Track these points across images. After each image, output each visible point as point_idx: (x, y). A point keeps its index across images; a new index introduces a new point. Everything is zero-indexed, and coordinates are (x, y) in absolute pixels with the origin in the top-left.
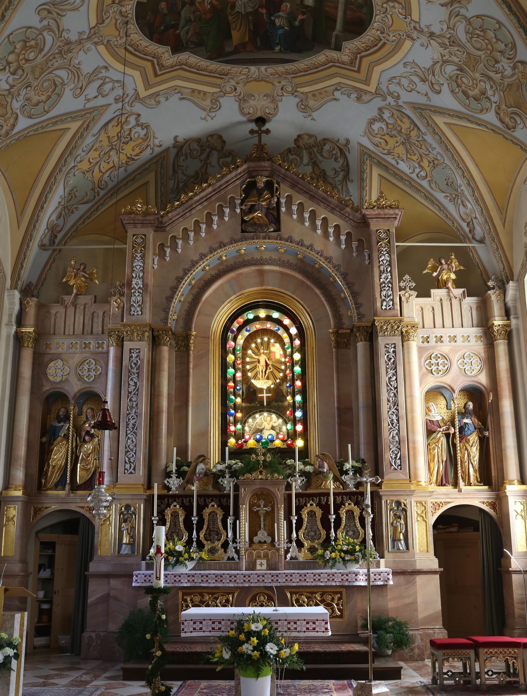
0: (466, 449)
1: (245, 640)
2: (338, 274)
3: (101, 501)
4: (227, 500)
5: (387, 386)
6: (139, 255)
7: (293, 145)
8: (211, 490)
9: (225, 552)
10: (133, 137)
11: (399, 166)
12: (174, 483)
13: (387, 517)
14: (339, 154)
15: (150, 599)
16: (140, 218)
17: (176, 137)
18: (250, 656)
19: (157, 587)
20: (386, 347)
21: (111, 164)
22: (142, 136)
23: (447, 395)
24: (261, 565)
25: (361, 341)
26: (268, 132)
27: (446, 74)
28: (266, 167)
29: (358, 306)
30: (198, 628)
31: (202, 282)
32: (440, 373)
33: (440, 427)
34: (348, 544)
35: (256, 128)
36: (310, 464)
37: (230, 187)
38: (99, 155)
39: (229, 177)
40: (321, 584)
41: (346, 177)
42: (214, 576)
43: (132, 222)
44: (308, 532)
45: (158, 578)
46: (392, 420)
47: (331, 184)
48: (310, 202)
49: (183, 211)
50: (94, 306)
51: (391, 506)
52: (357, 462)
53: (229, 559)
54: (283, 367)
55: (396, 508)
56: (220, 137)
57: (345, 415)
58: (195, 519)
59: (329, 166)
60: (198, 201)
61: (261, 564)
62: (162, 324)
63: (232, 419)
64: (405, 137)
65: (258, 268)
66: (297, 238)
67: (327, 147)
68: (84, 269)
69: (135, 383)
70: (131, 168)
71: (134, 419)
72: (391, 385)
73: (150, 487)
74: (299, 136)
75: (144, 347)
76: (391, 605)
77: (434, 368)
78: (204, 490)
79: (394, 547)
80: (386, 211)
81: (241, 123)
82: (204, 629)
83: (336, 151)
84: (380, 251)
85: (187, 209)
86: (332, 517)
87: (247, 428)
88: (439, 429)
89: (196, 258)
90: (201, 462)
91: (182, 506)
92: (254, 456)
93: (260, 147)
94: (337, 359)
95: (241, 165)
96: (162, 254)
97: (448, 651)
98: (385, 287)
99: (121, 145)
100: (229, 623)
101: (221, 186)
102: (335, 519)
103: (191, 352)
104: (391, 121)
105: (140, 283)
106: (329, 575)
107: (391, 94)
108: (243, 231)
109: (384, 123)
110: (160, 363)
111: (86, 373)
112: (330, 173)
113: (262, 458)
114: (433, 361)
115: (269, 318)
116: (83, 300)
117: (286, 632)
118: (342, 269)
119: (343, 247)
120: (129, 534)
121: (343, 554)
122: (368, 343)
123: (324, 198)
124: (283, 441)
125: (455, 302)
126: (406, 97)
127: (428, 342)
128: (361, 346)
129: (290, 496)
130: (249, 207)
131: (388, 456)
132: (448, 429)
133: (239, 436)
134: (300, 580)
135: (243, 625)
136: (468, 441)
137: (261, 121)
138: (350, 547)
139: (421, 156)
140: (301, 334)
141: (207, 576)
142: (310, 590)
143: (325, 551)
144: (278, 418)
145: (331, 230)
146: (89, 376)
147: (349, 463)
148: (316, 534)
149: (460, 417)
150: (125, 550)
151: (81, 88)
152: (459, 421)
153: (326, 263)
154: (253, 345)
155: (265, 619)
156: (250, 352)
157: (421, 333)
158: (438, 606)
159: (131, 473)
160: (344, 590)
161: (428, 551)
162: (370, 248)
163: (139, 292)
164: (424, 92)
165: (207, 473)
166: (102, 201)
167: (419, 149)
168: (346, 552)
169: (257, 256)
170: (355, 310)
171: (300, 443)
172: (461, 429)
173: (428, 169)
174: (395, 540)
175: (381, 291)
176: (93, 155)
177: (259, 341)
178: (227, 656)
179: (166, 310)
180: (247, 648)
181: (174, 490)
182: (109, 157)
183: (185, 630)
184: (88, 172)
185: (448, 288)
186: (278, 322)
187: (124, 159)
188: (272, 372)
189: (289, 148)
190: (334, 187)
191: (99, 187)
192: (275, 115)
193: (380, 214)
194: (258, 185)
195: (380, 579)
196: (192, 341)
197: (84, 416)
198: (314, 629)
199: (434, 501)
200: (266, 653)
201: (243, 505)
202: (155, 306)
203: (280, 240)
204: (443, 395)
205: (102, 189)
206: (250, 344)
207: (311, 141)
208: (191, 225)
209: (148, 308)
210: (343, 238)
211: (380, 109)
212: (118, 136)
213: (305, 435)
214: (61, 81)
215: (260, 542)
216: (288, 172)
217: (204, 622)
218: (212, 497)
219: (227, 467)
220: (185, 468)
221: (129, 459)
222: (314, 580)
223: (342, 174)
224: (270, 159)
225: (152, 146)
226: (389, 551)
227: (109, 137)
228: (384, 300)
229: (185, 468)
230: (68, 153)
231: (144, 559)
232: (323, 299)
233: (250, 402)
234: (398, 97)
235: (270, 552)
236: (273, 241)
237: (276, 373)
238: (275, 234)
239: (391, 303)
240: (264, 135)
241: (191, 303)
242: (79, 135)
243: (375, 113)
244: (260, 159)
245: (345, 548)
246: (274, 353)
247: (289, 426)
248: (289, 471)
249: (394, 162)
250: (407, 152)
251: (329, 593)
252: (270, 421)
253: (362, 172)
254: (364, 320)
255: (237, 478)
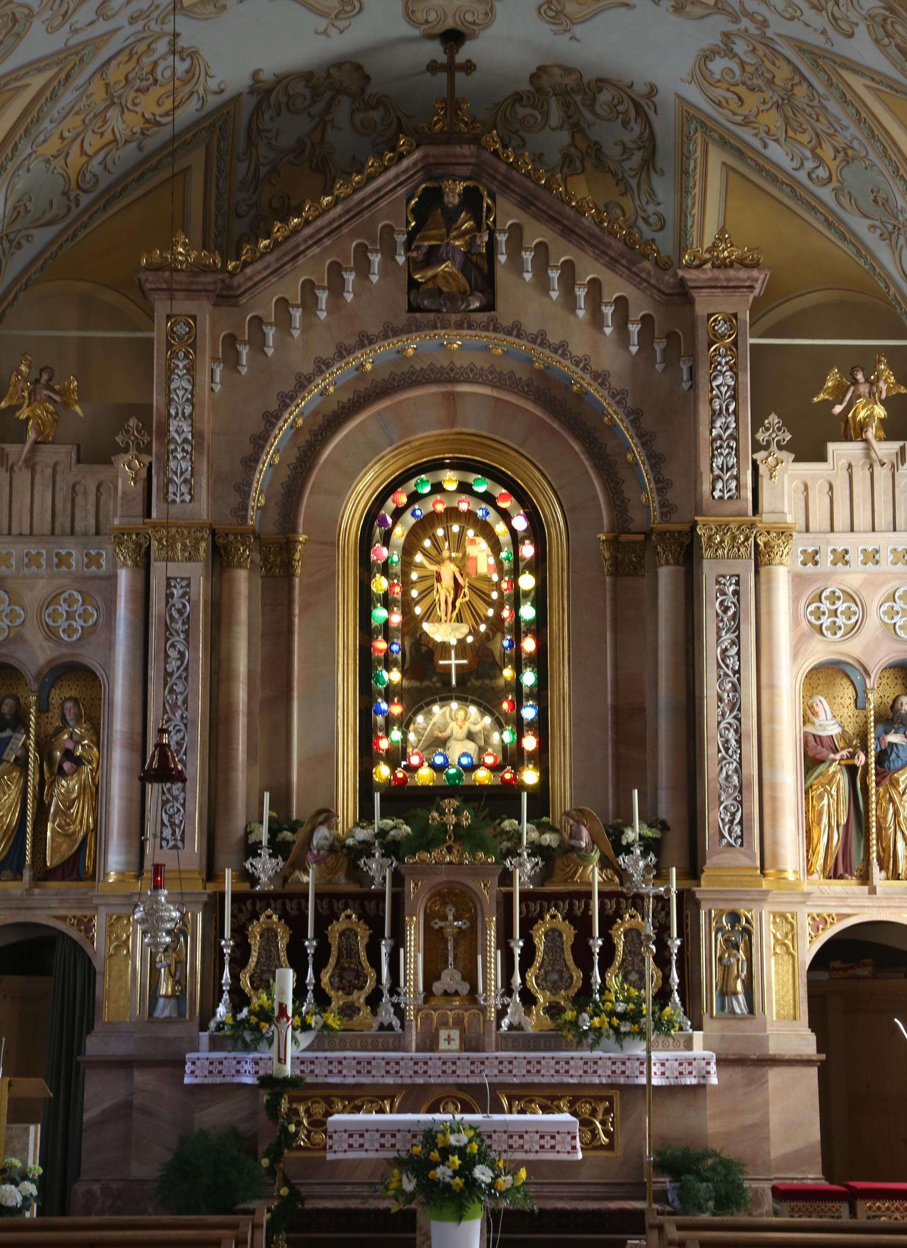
0: (891, 800)
1: (439, 1160)
2: (620, 411)
3: (161, 919)
4: (377, 905)
5: (719, 666)
6: (181, 365)
7: (526, 87)
8: (343, 884)
9: (374, 1012)
10: (159, 77)
11: (768, 153)
12: (265, 867)
13: (710, 945)
14: (632, 114)
15: (266, 1098)
16: (182, 277)
17: (255, 74)
18: (448, 1186)
19: (281, 1076)
20: (718, 582)
21: (108, 137)
22: (180, 72)
23: (857, 678)
24: (449, 1041)
25: (667, 563)
26: (469, 67)
27: (861, 8)
28: (464, 156)
29: (662, 485)
30: (356, 1145)
31: (319, 419)
32: (840, 633)
33: (836, 751)
34: (627, 1000)
35: (443, 58)
36: (552, 829)
37: (383, 204)
38: (84, 121)
39: (381, 180)
40: (571, 1081)
41: (649, 163)
42: (354, 1063)
43: (164, 286)
44: (546, 973)
45: (282, 1060)
46: (727, 741)
47: (614, 175)
48: (562, 242)
49: (277, 260)
50: (76, 468)
51: (719, 921)
52: (650, 826)
53: (382, 1027)
54: (495, 595)
55: (728, 927)
56: (359, 68)
57: (627, 726)
58: (310, 945)
59: (612, 136)
60: (311, 236)
61: (449, 1040)
62: (234, 521)
63: (380, 719)
64: (782, 93)
65: (443, 389)
66: (531, 328)
67: (605, 96)
68: (50, 380)
69: (180, 653)
70: (152, 143)
71: (179, 731)
72: (727, 666)
73: (212, 874)
74: (542, 69)
75: (195, 573)
76: (714, 1126)
77: (826, 621)
78: (329, 882)
79: (722, 1007)
80: (731, 273)
81: (405, 40)
82: (366, 1146)
83: (626, 106)
84: (713, 363)
85: (285, 254)
86: (597, 944)
87: (412, 737)
88: (832, 756)
89: (307, 368)
90: (321, 823)
91: (284, 915)
92: (435, 814)
93: (452, 104)
94: (615, 600)
95: (410, 153)
96: (231, 361)
97: (800, 1204)
98: (721, 447)
99: (132, 94)
100: (409, 1136)
101: (363, 200)
102: (601, 948)
103: (297, 580)
104: (749, 59)
105: (187, 428)
106: (586, 1063)
107: (751, 16)
108: (412, 309)
109: (736, 59)
110: (232, 607)
111: (62, 623)
112: (612, 151)
113: (453, 819)
114: (826, 606)
115: (464, 488)
116: (49, 454)
117: (505, 1151)
118: (629, 402)
119: (634, 349)
120: (173, 976)
121: (615, 1021)
122: (682, 569)
123: (593, 235)
124: (495, 769)
125: (882, 474)
126: (777, 26)
127: (816, 563)
128: (666, 576)
129: (509, 897)
130: (424, 250)
131: (715, 816)
132: (852, 755)
133: (396, 757)
134: (529, 1071)
135: (434, 1138)
136: (895, 784)
137: (453, 38)
138: (631, 1006)
139: (817, 135)
140: (537, 532)
141: (340, 1063)
142: (547, 1093)
143: (579, 1013)
144: (483, 715)
145: (608, 311)
146: (69, 630)
147: (633, 827)
148: (561, 977)
149: (881, 728)
150: (164, 1010)
151: (64, 16)
152: (877, 738)
153: (595, 385)
154: (427, 543)
155: (471, 1127)
156: (419, 558)
157: (800, 543)
158: (814, 1133)
159: (175, 847)
160: (617, 1095)
161: (795, 1018)
162: (693, 354)
163: (183, 450)
164: (821, 28)
165: (336, 847)
166: (85, 218)
167: (813, 122)
168: (622, 1016)
169: (443, 361)
170: (655, 495)
171: (530, 776)
172: (883, 757)
173: (833, 165)
174: (726, 993)
175: (713, 456)
176: (74, 122)
177: (440, 532)
178: (409, 1185)
179: (244, 488)
180: (442, 1173)
181: (265, 883)
182: (105, 122)
183: (335, 1147)
184: (55, 157)
185: (866, 441)
186: (488, 498)
187: (137, 123)
188: (469, 604)
189: (516, 93)
190: (620, 180)
191: (79, 187)
192: (488, 25)
193: (716, 279)
194: (446, 199)
195: (690, 1073)
196: (297, 556)
197: (55, 712)
198: (553, 1147)
199: (815, 911)
200: (475, 1180)
201: (411, 916)
202: (216, 478)
203: (495, 330)
204: (848, 677)
205: (86, 191)
206: (421, 540)
207: (570, 81)
208: (295, 294)
209: (205, 487)
210: (634, 329)
211: (726, 35)
212: (126, 78)
213: (541, 758)
214: (26, 11)
215: (446, 993)
216: (514, 173)
217: (367, 1135)
218: (347, 898)
219: (376, 836)
220: (287, 835)
221: (171, 816)
222: (557, 1072)
223: (638, 156)
224: (475, 140)
225: (201, 92)
226: (711, 1016)
227: (107, 85)
228: (719, 477)
229: (287, 835)
230: (22, 131)
231: (204, 1027)
232: (587, 463)
233: (421, 679)
234: (765, 23)
235: (466, 1014)
236: (479, 333)
237: (479, 605)
238: (483, 317)
239: (733, 484)
240: (460, 76)
241: (295, 468)
242: (49, 94)
243: (716, 40)
244: (450, 138)
245: (620, 1008)
246: (475, 559)
247: (508, 737)
248: (506, 845)
249: (757, 143)
250: (787, 124)
251: (588, 1099)
252: (465, 719)
253: (685, 157)
254: (674, 517)
255: (400, 860)
